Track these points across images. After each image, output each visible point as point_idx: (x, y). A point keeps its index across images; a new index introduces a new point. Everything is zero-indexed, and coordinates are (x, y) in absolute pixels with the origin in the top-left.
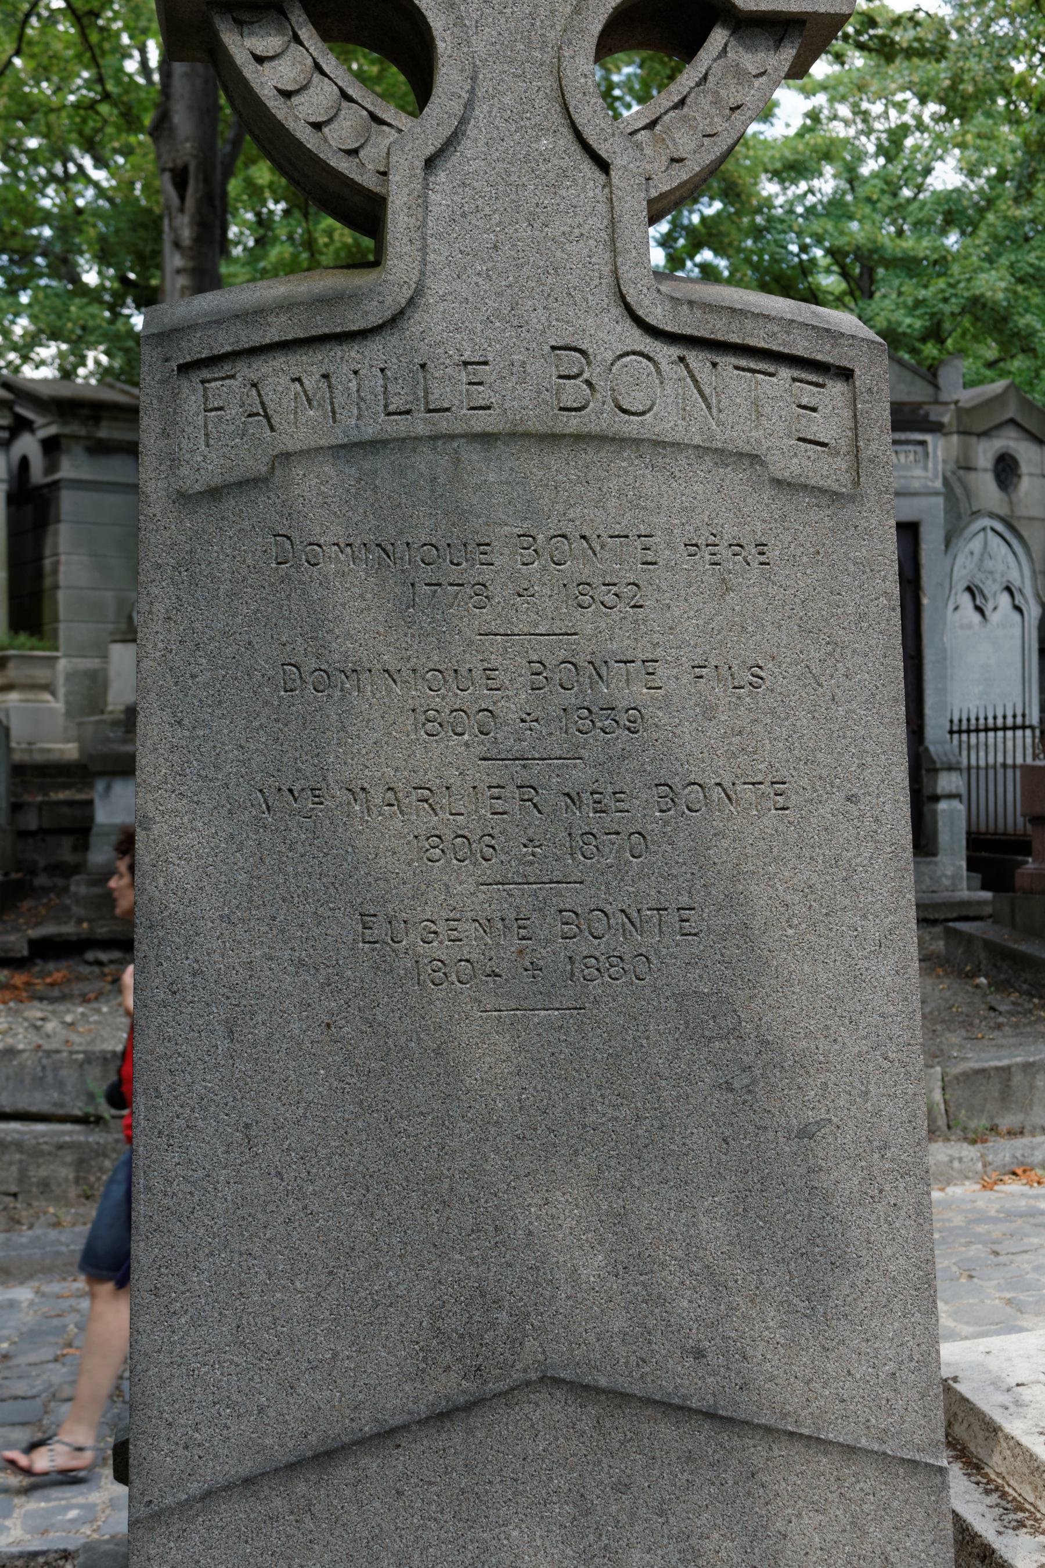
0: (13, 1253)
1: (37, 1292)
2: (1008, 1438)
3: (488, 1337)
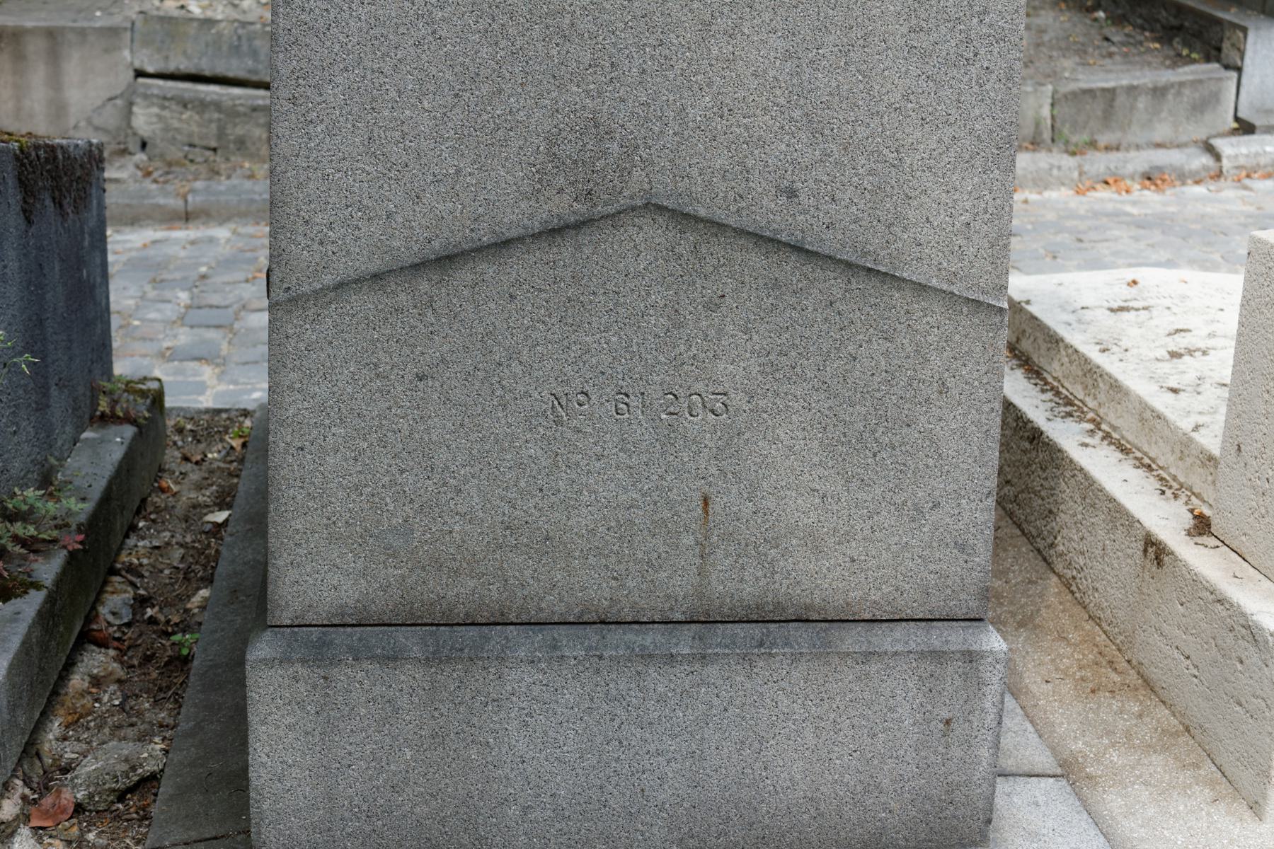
0: (213, 198)
1: (234, 232)
2: (1067, 346)
3: (599, 165)
